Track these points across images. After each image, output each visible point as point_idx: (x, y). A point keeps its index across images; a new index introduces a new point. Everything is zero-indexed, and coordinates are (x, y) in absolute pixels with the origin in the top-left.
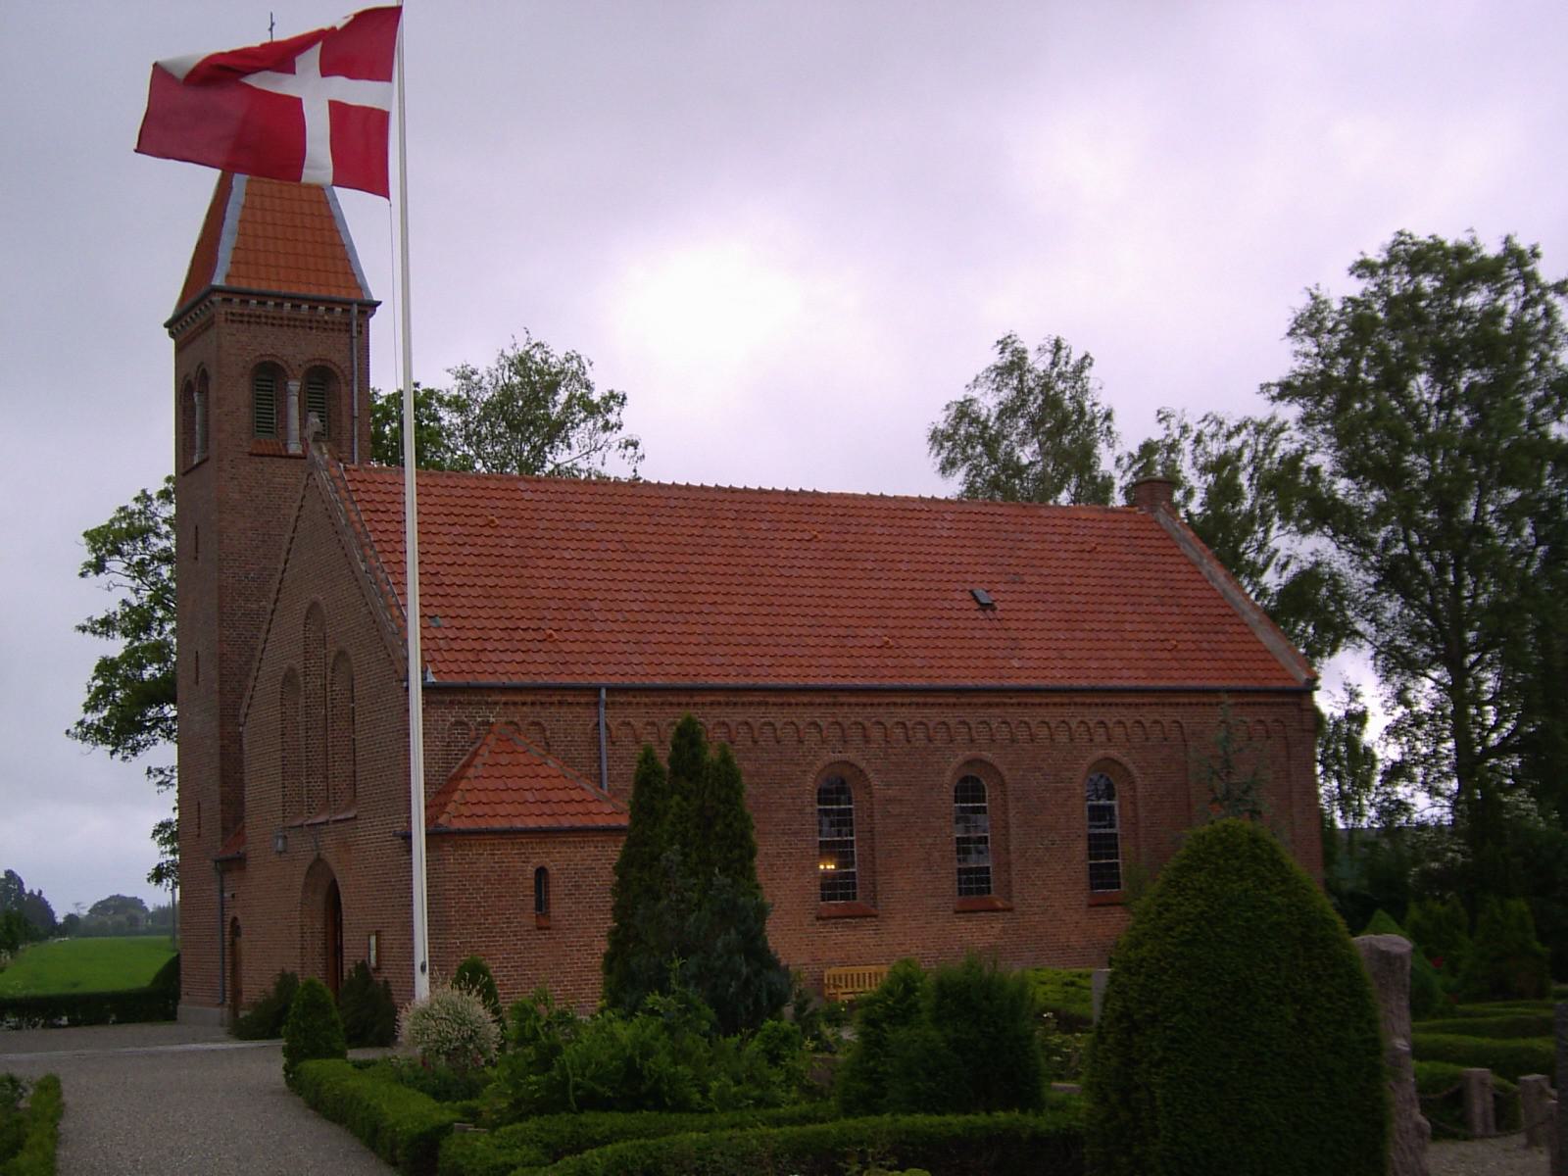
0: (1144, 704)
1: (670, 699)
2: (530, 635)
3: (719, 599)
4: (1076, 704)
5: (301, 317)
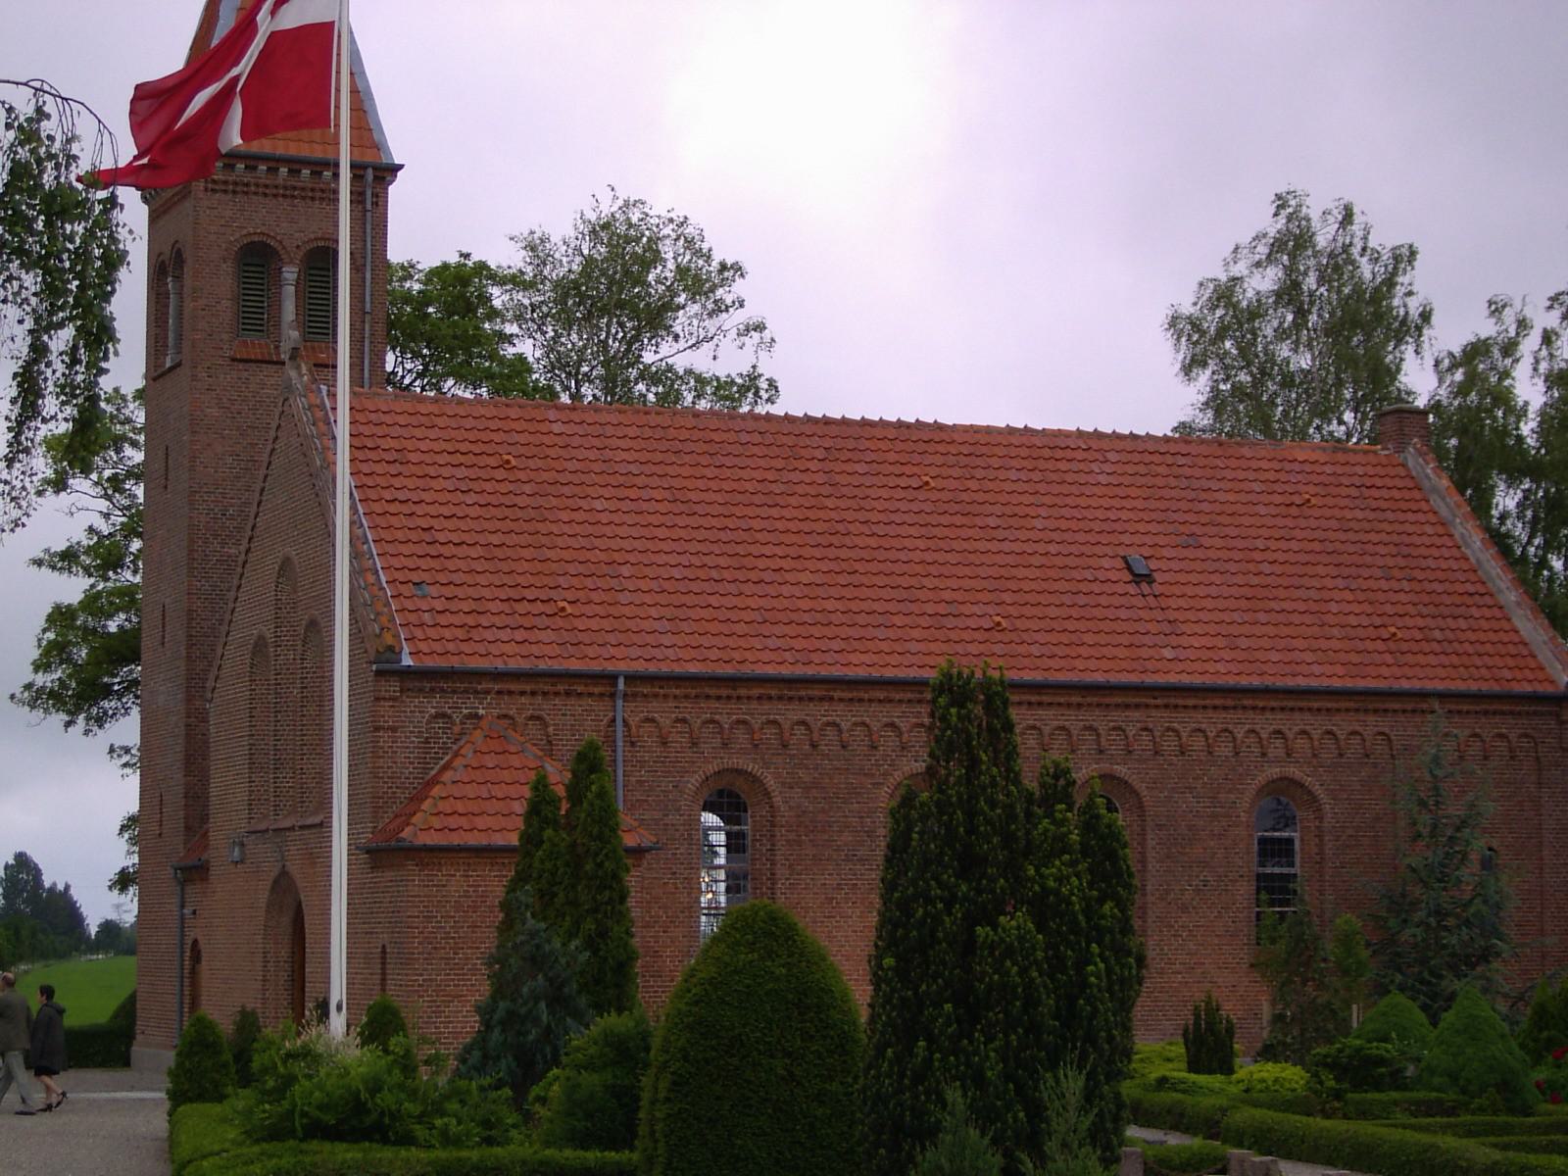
0: (1338, 710)
1: (707, 690)
2: (539, 607)
3: (786, 564)
4: (1244, 708)
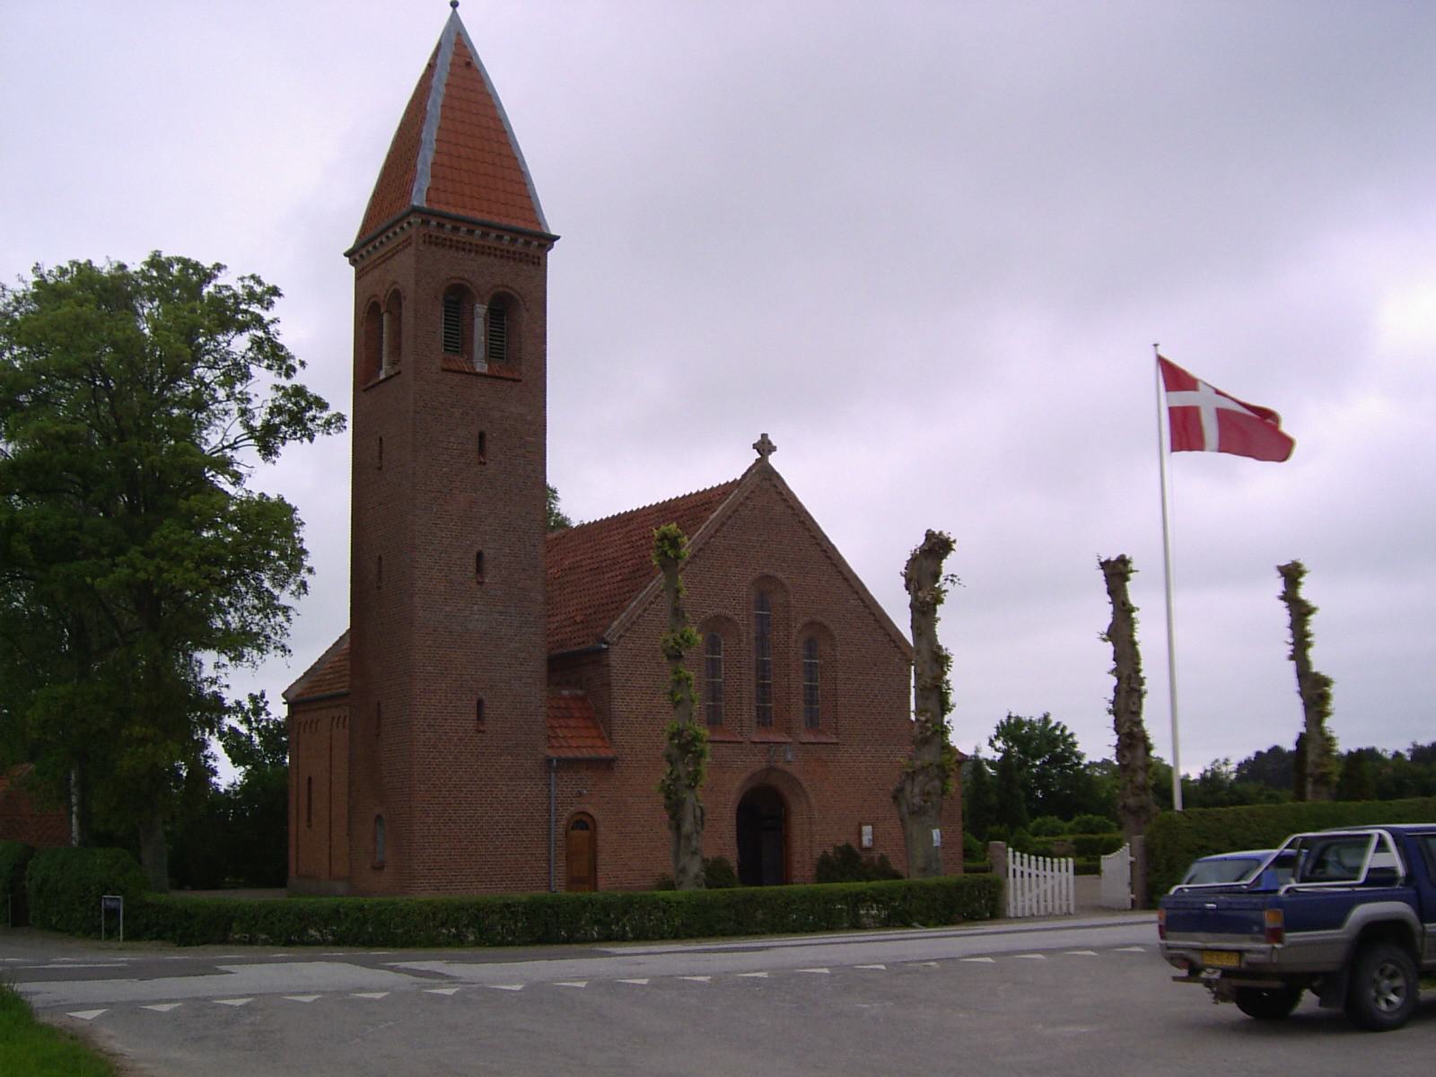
5: (502, 247)
